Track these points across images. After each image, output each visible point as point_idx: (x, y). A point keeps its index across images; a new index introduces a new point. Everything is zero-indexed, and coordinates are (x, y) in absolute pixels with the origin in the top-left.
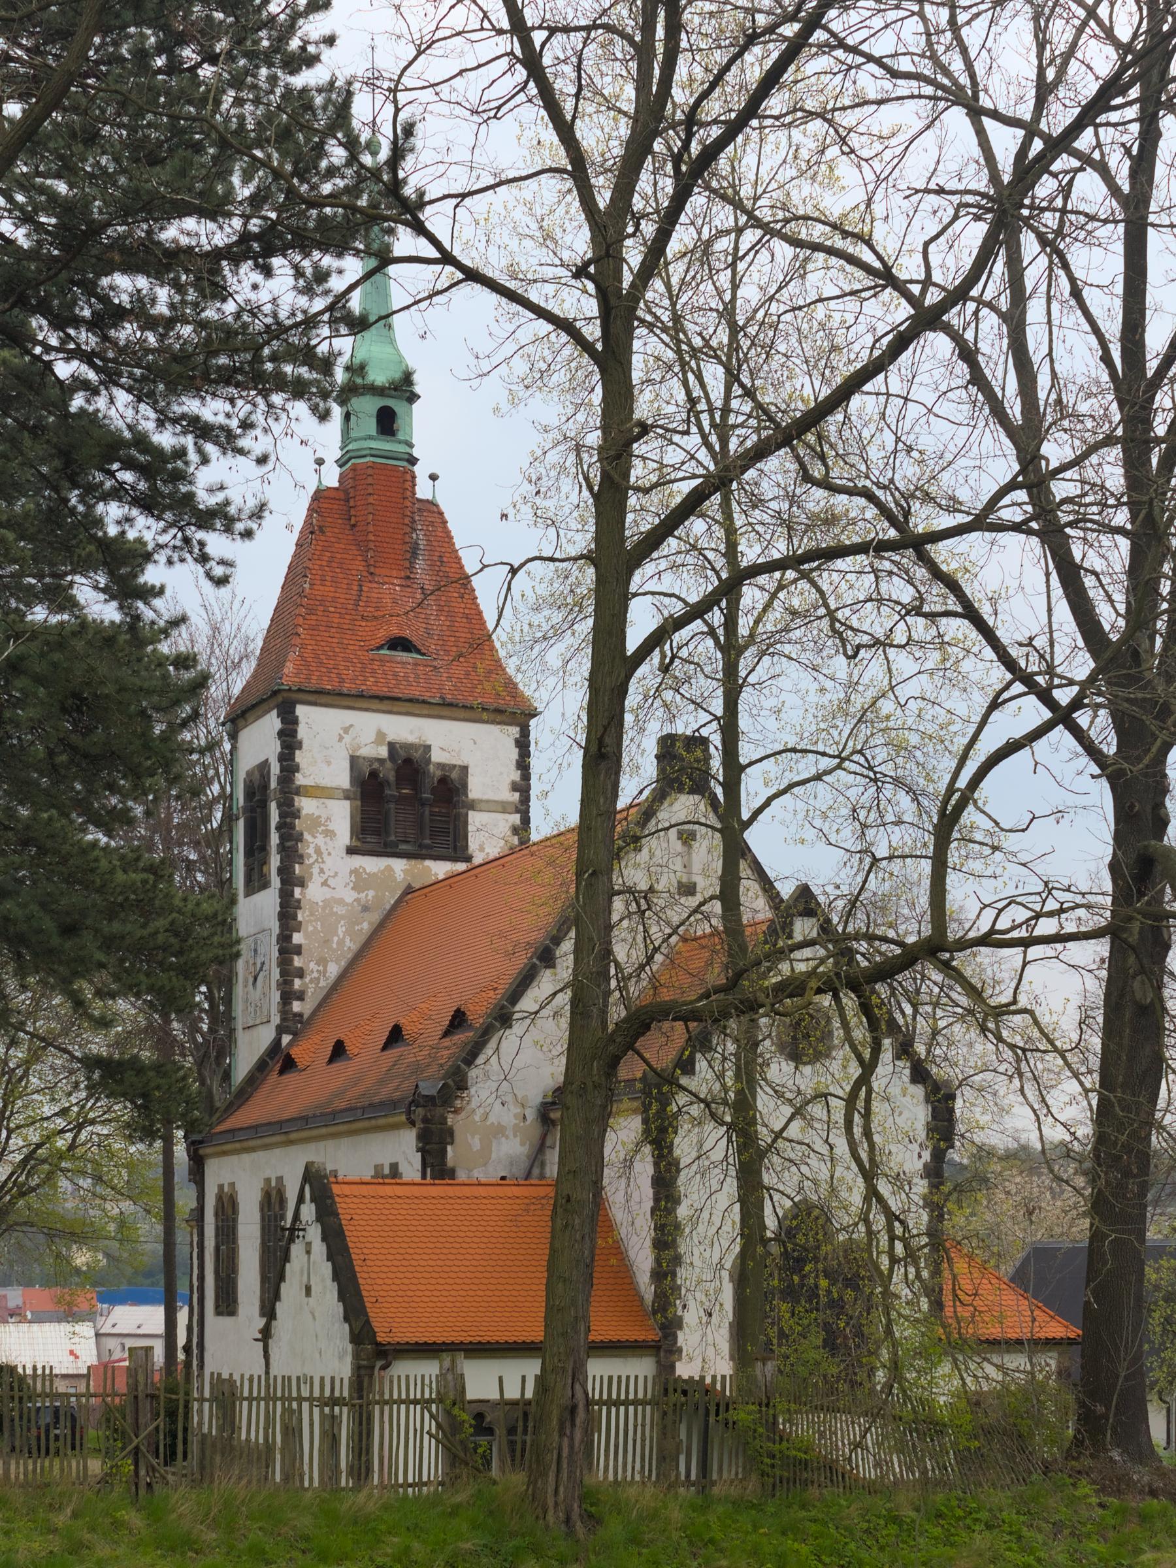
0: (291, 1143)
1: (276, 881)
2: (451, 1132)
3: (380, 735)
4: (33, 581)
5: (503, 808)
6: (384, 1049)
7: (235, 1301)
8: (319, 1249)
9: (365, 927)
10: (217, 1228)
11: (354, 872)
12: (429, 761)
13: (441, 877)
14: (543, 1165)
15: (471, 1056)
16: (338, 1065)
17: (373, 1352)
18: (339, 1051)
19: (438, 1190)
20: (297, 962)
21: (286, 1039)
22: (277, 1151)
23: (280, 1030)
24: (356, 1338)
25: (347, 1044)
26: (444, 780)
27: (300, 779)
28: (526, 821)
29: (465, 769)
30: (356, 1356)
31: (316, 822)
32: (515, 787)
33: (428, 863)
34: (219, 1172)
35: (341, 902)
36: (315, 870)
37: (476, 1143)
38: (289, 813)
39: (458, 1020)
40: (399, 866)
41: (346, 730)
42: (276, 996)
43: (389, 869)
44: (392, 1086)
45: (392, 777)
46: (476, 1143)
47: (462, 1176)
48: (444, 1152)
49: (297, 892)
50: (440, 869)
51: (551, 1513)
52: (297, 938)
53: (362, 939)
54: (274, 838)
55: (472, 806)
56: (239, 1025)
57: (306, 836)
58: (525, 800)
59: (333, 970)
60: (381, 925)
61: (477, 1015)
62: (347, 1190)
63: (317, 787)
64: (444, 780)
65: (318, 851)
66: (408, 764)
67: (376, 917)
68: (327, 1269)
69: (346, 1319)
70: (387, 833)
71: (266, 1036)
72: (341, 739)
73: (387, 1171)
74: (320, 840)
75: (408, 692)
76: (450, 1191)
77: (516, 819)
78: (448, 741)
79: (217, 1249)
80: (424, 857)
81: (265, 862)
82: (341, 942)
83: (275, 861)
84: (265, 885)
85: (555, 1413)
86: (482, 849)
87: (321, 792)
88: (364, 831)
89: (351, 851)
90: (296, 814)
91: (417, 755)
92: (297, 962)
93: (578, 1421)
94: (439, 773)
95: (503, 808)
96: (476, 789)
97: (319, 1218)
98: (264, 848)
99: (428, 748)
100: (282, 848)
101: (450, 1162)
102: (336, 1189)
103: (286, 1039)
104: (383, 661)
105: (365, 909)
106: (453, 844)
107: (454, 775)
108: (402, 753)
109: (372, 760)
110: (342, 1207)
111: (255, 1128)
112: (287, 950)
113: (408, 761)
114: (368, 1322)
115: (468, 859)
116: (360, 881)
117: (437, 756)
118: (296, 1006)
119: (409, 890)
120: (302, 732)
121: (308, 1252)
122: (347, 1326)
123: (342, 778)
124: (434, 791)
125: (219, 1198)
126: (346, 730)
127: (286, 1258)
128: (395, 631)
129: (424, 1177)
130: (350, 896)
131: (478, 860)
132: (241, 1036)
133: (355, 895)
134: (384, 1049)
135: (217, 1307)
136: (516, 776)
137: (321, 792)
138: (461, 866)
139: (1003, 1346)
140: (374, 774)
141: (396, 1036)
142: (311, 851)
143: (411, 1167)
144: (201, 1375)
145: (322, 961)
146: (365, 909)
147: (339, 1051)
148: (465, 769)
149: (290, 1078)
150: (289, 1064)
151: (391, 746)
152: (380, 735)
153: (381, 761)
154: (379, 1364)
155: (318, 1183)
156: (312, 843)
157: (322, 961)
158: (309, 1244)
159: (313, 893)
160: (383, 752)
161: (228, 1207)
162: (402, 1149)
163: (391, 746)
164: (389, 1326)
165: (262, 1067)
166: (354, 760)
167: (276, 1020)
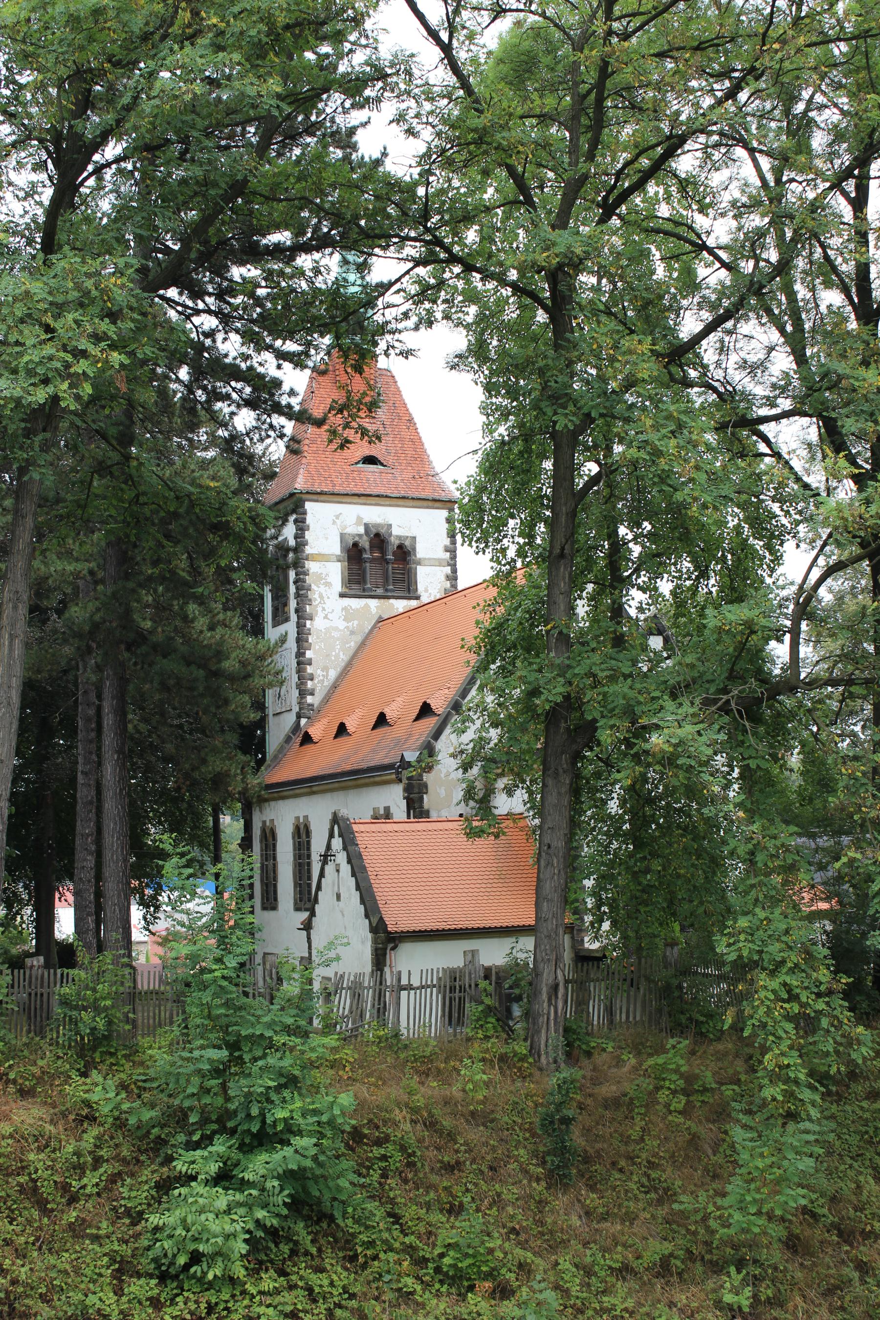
0: (314, 793)
1: (294, 617)
2: (426, 786)
3: (359, 519)
5: (439, 563)
6: (374, 728)
8: (346, 869)
9: (353, 645)
11: (344, 609)
12: (390, 535)
13: (401, 610)
16: (342, 740)
17: (386, 940)
18: (342, 730)
20: (309, 670)
22: (304, 799)
23: (299, 716)
24: (374, 930)
25: (348, 725)
26: (401, 547)
27: (308, 550)
28: (454, 571)
29: (414, 538)
30: (375, 941)
31: (319, 577)
32: (447, 550)
33: (392, 601)
35: (336, 629)
36: (319, 609)
37: (442, 792)
38: (302, 573)
39: (426, 710)
40: (373, 603)
41: (337, 517)
42: (295, 693)
43: (367, 605)
44: (382, 754)
45: (367, 546)
46: (442, 792)
47: (434, 815)
48: (422, 799)
49: (308, 623)
50: (400, 605)
51: (543, 1058)
52: (309, 654)
53: (351, 653)
54: (292, 589)
55: (419, 563)
56: (270, 711)
57: (313, 587)
58: (454, 557)
59: (333, 674)
60: (363, 644)
61: (439, 704)
62: (362, 828)
63: (320, 554)
64: (401, 547)
65: (321, 596)
66: (378, 538)
67: (359, 638)
68: (352, 882)
69: (367, 916)
70: (365, 582)
72: (334, 523)
73: (382, 812)
74: (322, 589)
75: (375, 492)
77: (448, 570)
78: (401, 522)
80: (388, 598)
81: (286, 604)
82: (337, 656)
83: (293, 604)
84: (287, 620)
85: (544, 990)
86: (426, 591)
87: (322, 558)
88: (350, 581)
89: (342, 595)
90: (306, 573)
91: (383, 531)
92: (309, 670)
93: (560, 995)
94: (397, 542)
95: (439, 563)
96: (421, 552)
97: (345, 848)
98: (286, 596)
99: (390, 526)
100: (298, 595)
102: (355, 828)
104: (360, 471)
105: (352, 633)
106: (408, 589)
107: (407, 543)
108: (374, 531)
109: (354, 536)
110: (360, 839)
112: (302, 663)
113: (377, 535)
114: (381, 919)
115: (418, 598)
116: (348, 615)
117: (396, 531)
118: (309, 699)
119: (381, 620)
120: (309, 519)
123: (335, 548)
124: (394, 554)
125: (263, 830)
126: (337, 517)
128: (367, 453)
129: (409, 817)
130: (342, 625)
131: (425, 599)
132: (271, 720)
133: (345, 624)
134: (374, 728)
135: (263, 903)
136: (447, 541)
137: (322, 558)
138: (414, 603)
140: (355, 545)
141: (381, 720)
142: (316, 596)
143: (399, 808)
145: (326, 669)
146: (352, 633)
147: (342, 730)
148: (414, 538)
149: (309, 747)
150: (307, 739)
151: (366, 526)
152: (359, 519)
153: (360, 536)
154: (391, 945)
155: (340, 825)
156: (317, 592)
157: (326, 669)
158: (338, 865)
159: (317, 625)
160: (362, 530)
161: (269, 837)
162: (394, 797)
163: (366, 526)
164: (397, 919)
165: (288, 740)
166: (342, 536)
167: (296, 709)
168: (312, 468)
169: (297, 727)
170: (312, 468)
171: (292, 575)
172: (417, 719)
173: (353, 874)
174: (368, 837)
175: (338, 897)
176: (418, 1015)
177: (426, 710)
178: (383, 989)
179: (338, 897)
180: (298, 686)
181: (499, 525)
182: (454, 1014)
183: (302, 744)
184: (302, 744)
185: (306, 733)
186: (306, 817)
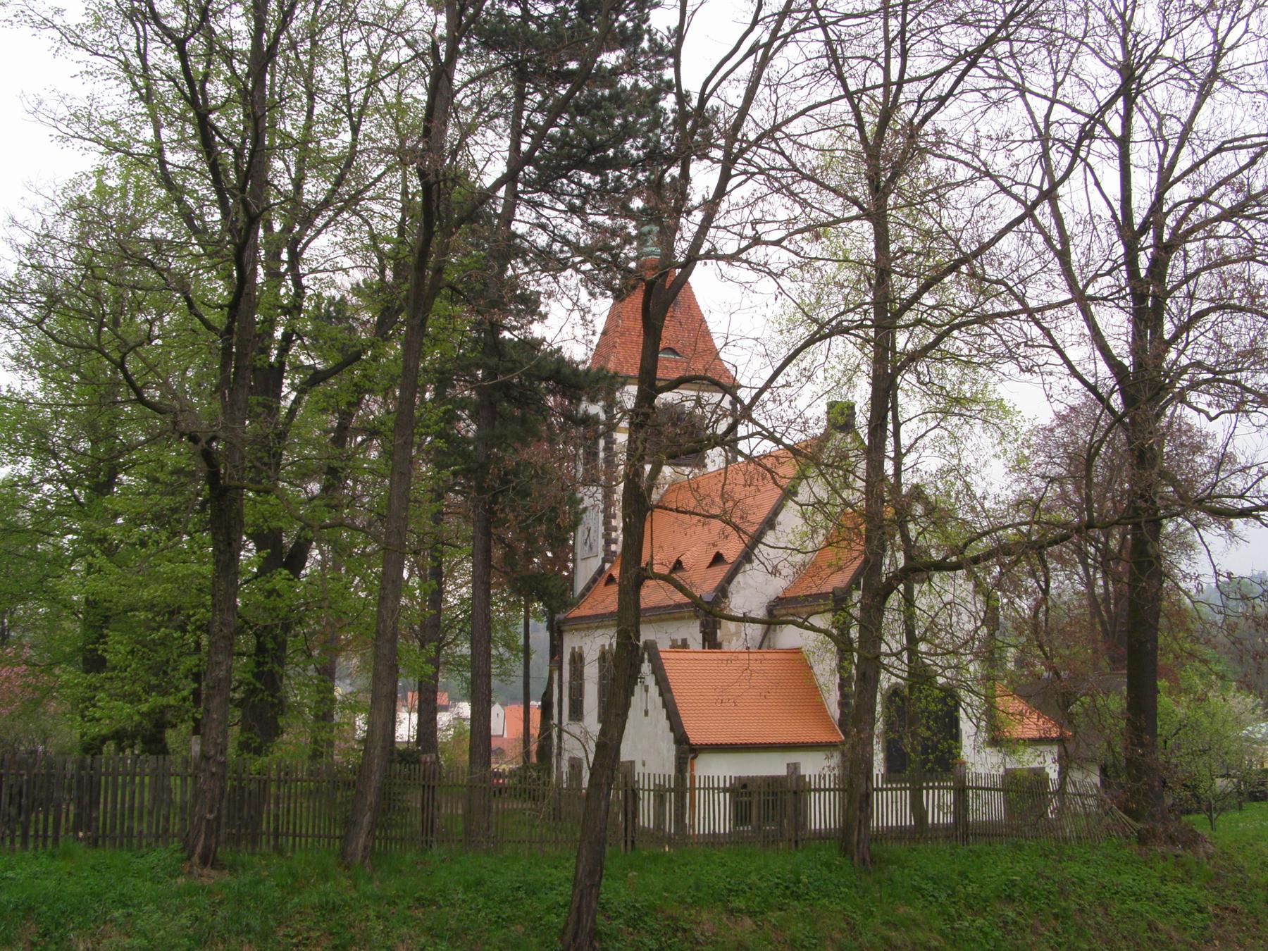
4: (690, 123)
7: (582, 713)
8: (654, 690)
10: (602, 677)
14: (844, 646)
15: (730, 578)
17: (687, 750)
19: (714, 656)
21: (607, 566)
23: (604, 561)
30: (678, 751)
34: (570, 643)
39: (718, 559)
47: (725, 647)
68: (659, 700)
71: (595, 564)
73: (680, 643)
76: (719, 656)
79: (570, 682)
101: (719, 640)
102: (662, 655)
103: (607, 566)
111: (596, 616)
118: (613, 547)
121: (647, 691)
122: (672, 735)
125: (573, 655)
127: (632, 694)
135: (570, 716)
139: (667, 696)
144: (560, 754)
154: (691, 756)
161: (578, 660)
165: (594, 580)
167: (602, 555)
168: (620, 356)
169: (601, 571)
170: (620, 356)
171: (602, 443)
172: (710, 566)
173: (661, 694)
174: (673, 663)
175: (646, 713)
176: (712, 815)
177: (718, 559)
178: (680, 788)
179: (646, 713)
180: (604, 536)
181: (1170, 424)
182: (741, 813)
183: (606, 584)
184: (606, 584)
185: (611, 575)
186: (581, 648)
